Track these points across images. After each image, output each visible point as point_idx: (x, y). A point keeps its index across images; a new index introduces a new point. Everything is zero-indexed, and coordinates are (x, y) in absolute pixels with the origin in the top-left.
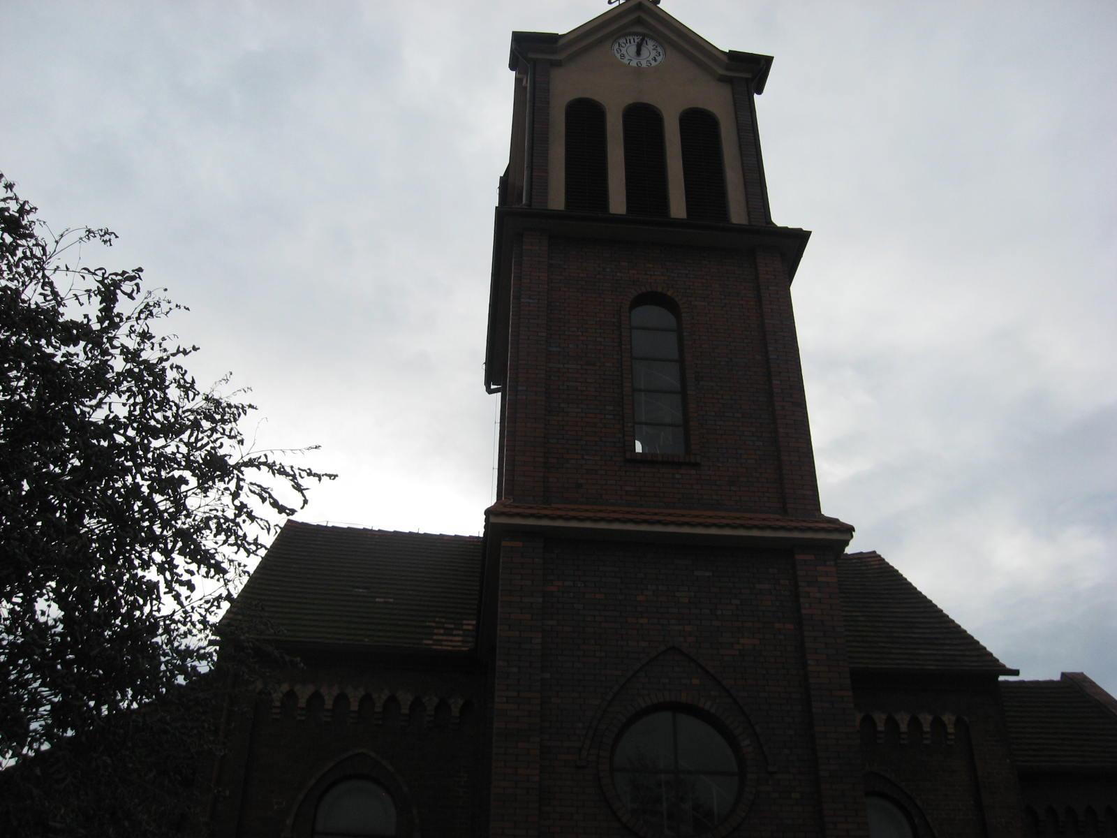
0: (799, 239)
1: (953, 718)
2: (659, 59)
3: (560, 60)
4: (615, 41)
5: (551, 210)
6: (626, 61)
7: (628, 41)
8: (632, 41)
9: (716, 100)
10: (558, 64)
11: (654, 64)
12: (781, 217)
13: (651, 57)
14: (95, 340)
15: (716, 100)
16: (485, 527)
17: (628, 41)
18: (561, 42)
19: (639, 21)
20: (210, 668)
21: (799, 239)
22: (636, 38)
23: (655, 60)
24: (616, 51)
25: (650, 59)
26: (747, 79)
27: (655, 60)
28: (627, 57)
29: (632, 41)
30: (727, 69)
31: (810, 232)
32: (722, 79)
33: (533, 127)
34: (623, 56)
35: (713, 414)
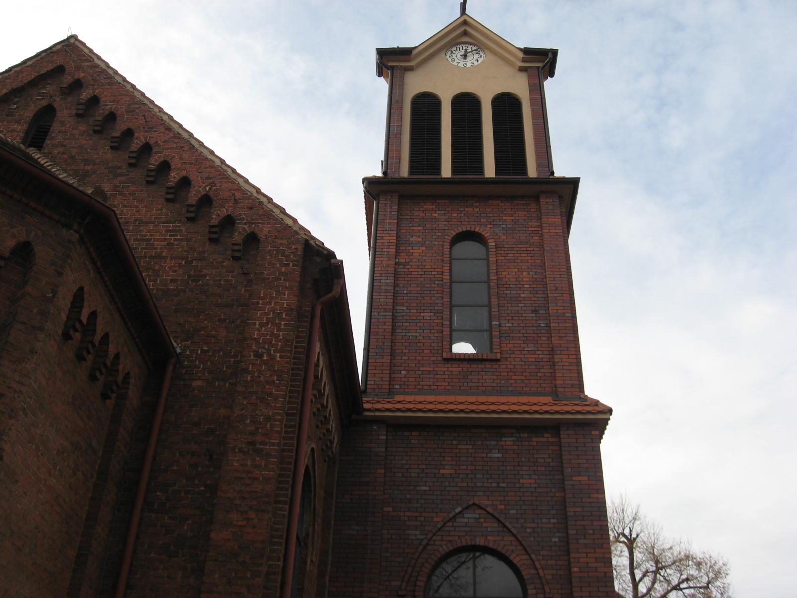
0: (573, 184)
2: (480, 60)
3: (413, 66)
4: (448, 50)
5: (531, 178)
6: (455, 64)
7: (458, 49)
8: (461, 48)
9: (519, 86)
10: (411, 69)
11: (476, 63)
12: (561, 169)
13: (475, 59)
14: (395, 353)
15: (519, 86)
16: (604, 433)
17: (458, 49)
18: (414, 52)
19: (465, 33)
20: (615, 535)
21: (573, 184)
22: (464, 46)
23: (478, 61)
24: (448, 56)
25: (474, 60)
26: (538, 68)
27: (478, 61)
28: (457, 60)
29: (461, 48)
30: (524, 60)
31: (580, 178)
32: (522, 69)
33: (544, 120)
34: (453, 60)
35: (532, 381)
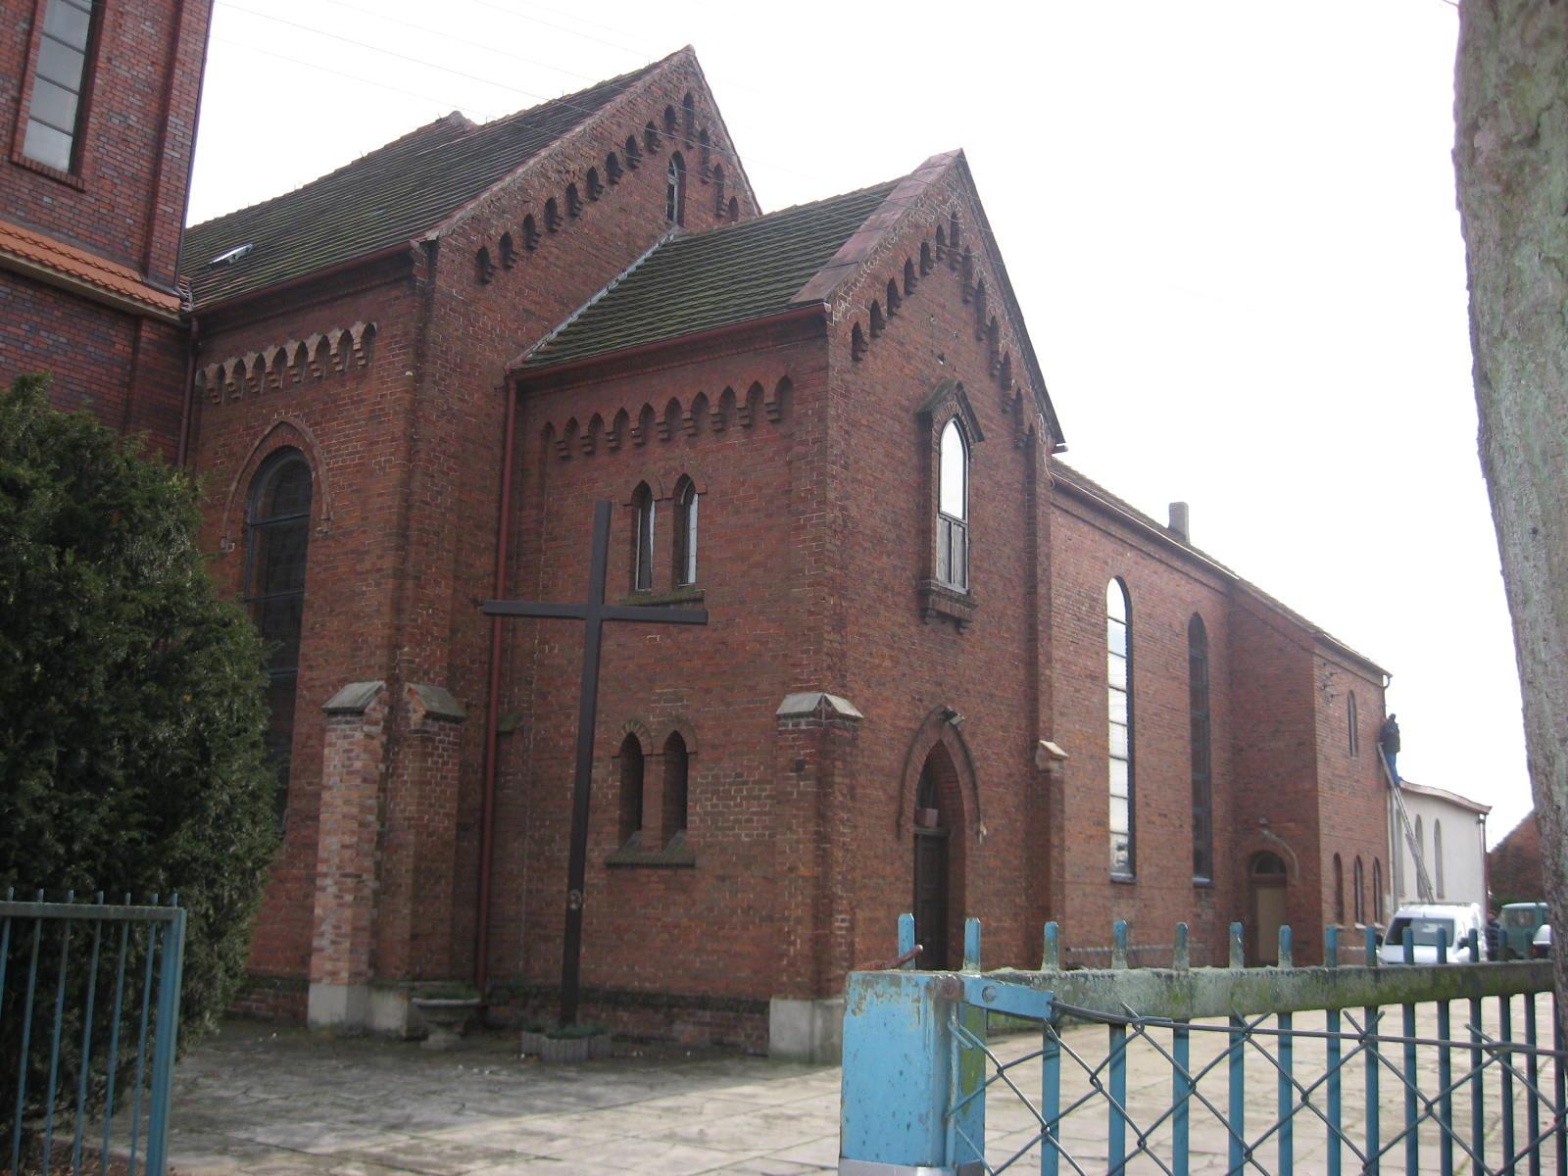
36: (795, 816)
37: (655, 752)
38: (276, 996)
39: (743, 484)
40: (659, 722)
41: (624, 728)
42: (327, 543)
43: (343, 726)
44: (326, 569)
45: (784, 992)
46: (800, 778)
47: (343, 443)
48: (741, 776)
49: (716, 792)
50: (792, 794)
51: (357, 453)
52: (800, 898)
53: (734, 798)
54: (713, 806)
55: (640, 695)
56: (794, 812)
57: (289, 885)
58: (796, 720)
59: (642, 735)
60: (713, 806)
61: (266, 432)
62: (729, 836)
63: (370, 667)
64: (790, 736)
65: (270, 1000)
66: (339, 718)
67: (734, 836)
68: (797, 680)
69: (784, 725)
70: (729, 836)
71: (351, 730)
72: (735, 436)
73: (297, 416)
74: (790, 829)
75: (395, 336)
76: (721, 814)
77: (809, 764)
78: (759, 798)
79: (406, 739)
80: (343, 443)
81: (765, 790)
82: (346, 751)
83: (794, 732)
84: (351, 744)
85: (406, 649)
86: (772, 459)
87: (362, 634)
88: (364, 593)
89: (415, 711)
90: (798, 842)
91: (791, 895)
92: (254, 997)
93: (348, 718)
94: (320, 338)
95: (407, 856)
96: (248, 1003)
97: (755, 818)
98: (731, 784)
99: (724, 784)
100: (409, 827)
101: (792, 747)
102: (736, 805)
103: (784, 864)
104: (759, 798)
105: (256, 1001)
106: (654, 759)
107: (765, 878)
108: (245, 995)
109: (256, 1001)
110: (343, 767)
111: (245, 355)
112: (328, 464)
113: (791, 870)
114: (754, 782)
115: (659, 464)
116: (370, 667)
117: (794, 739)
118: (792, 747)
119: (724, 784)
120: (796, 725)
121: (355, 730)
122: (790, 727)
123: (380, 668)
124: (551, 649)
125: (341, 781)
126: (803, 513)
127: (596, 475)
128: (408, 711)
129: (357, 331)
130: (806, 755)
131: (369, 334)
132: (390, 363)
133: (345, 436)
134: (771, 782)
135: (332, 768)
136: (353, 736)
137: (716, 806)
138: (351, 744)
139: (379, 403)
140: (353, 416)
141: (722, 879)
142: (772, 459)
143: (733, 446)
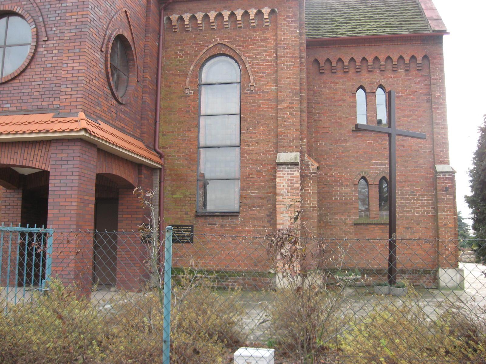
1: (269, 10)
36: (446, 207)
37: (375, 183)
38: (243, 279)
39: (406, 90)
40: (375, 173)
41: (360, 174)
42: (253, 95)
43: (286, 170)
44: (253, 106)
45: (444, 267)
46: (447, 194)
47: (258, 55)
48: (413, 192)
49: (403, 198)
50: (444, 199)
51: (267, 60)
52: (449, 234)
53: (411, 200)
54: (401, 203)
55: (365, 163)
56: (445, 205)
57: (243, 234)
58: (444, 174)
59: (368, 177)
60: (401, 203)
61: (210, 47)
62: (409, 213)
63: (290, 147)
64: (442, 179)
65: (241, 281)
66: (284, 166)
67: (412, 213)
68: (439, 160)
69: (439, 175)
70: (409, 213)
71: (291, 171)
72: (401, 73)
73: (228, 42)
74: (444, 211)
75: (289, 16)
76: (405, 206)
77: (450, 189)
78: (421, 200)
79: (308, 176)
80: (258, 55)
81: (424, 198)
82: (289, 180)
83: (443, 178)
84: (292, 177)
85: (305, 140)
86: (418, 83)
87: (284, 133)
88: (284, 117)
89: (312, 165)
90: (447, 215)
91: (445, 233)
92: (229, 280)
93: (289, 166)
94: (243, 11)
95: (313, 222)
96: (227, 283)
97: (420, 207)
98: (409, 195)
99: (406, 195)
100: (313, 210)
101: (443, 183)
102: (412, 203)
103: (442, 223)
104: (421, 200)
105: (230, 282)
106: (374, 186)
107: (426, 228)
108: (225, 280)
109: (230, 282)
110: (288, 186)
111: (197, 13)
112: (249, 63)
113: (445, 225)
114: (419, 195)
115: (367, 80)
116: (290, 147)
117: (443, 180)
118: (443, 183)
119: (406, 195)
120: (445, 175)
121: (295, 171)
122: (442, 176)
123: (296, 147)
124: (320, 144)
125: (288, 192)
126: (438, 103)
127: (337, 81)
128: (308, 165)
129: (266, 11)
130: (448, 186)
131: (273, 12)
132: (287, 26)
133: (258, 53)
134: (426, 195)
135: (282, 187)
136: (293, 174)
137: (403, 203)
138: (292, 177)
139: (283, 41)
140: (263, 45)
141: (407, 228)
142: (418, 83)
143: (401, 77)
